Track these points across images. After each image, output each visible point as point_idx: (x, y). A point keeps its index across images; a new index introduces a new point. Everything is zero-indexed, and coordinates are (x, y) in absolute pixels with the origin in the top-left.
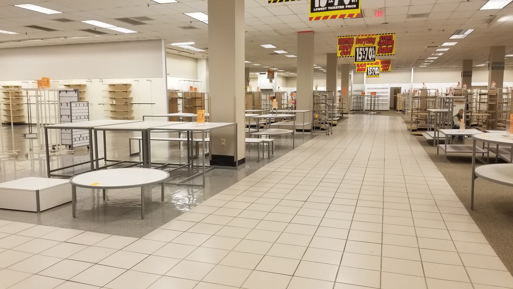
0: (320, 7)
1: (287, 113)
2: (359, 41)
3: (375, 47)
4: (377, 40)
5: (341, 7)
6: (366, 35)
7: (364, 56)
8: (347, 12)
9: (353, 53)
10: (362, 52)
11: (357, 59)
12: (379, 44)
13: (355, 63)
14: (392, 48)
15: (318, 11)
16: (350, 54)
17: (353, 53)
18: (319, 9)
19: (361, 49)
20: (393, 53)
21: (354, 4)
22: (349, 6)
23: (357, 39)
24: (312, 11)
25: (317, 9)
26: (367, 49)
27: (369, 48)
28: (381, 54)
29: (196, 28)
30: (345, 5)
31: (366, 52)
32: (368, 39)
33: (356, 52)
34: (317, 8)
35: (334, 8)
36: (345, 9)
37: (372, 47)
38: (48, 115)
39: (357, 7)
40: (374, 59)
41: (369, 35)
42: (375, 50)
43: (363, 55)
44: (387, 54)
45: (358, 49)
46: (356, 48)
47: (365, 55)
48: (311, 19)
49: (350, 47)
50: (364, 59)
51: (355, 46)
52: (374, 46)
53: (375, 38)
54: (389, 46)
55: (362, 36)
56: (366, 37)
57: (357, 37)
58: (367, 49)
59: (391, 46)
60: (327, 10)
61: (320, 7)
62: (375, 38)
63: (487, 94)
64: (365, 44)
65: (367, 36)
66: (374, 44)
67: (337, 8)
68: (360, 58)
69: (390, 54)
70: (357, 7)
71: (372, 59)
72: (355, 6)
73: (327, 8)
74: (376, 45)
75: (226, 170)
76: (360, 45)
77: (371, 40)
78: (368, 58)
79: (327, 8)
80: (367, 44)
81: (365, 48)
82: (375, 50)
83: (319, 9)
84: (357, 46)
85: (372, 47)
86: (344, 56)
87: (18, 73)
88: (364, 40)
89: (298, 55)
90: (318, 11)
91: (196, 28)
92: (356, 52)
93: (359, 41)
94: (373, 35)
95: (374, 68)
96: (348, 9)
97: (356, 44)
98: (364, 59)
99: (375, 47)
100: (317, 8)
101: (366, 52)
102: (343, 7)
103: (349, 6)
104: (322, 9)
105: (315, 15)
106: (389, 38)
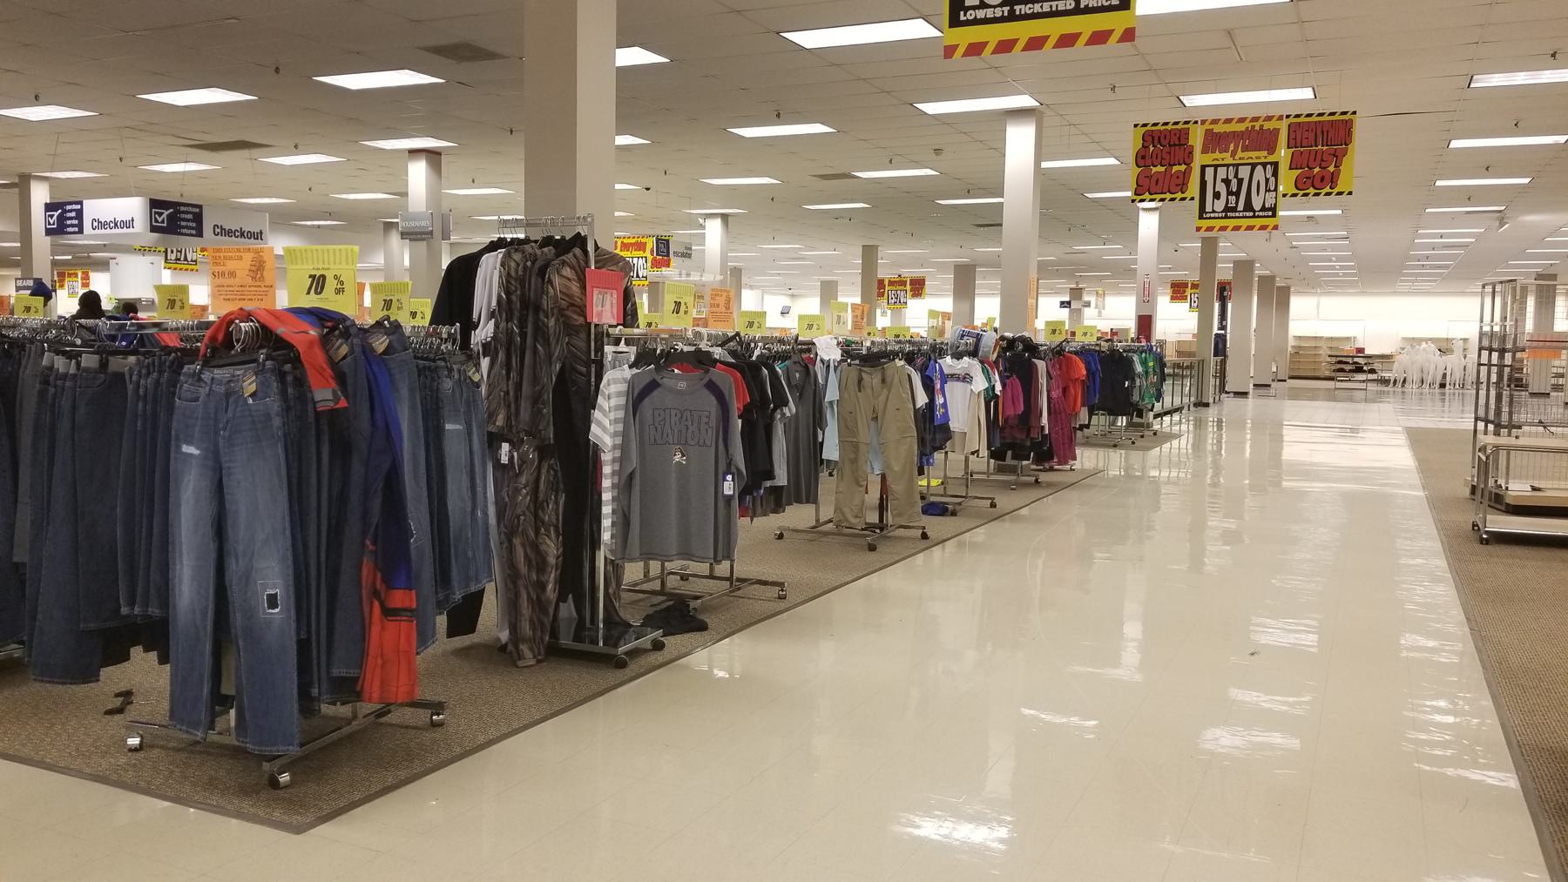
1: (485, 478)
8: (1258, 222)
9: (1193, 188)
10: (1227, 182)
11: (1209, 208)
17: (1193, 188)
18: (981, 14)
19: (1222, 173)
23: (1209, 133)
24: (1201, 217)
25: (971, 15)
26: (1244, 172)
27: (1254, 166)
31: (1240, 181)
33: (1203, 184)
34: (974, 8)
37: (1264, 165)
38: (1488, 300)
41: (1255, 119)
42: (1275, 174)
43: (1230, 193)
44: (1169, 196)
45: (1209, 172)
46: (1203, 168)
47: (1237, 194)
50: (1234, 209)
52: (1271, 159)
54: (1175, 169)
56: (1241, 127)
57: (1207, 126)
59: (1183, 167)
60: (1012, 17)
64: (1240, 154)
65: (1248, 124)
66: (1272, 149)
68: (1220, 205)
69: (1179, 195)
70: (1274, 215)
71: (1263, 209)
73: (1012, 11)
76: (1217, 155)
78: (1249, 206)
79: (1012, 11)
80: (1246, 154)
83: (981, 14)
84: (1208, 159)
85: (1264, 165)
86: (1312, 191)
92: (1203, 184)
95: (1244, 172)
97: (1205, 151)
98: (1234, 209)
99: (1276, 165)
100: (974, 8)
104: (989, 13)
105: (1205, 223)
106: (1175, 140)
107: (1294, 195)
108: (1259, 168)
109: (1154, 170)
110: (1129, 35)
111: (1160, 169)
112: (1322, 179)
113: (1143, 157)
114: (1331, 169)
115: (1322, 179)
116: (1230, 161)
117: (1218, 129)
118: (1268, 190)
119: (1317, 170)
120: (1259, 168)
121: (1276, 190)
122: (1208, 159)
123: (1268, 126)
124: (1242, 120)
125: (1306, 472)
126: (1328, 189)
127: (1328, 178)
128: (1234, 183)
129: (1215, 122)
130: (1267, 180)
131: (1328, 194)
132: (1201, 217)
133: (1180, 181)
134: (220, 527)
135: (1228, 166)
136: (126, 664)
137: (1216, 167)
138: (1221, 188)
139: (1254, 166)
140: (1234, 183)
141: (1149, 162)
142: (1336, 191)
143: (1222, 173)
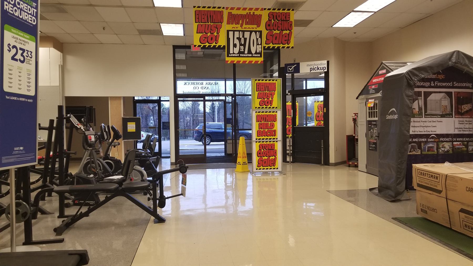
0: (234, 53)
2: (233, 19)
3: (261, 32)
4: (265, 19)
5: (249, 55)
6: (245, 9)
7: (242, 47)
10: (239, 39)
11: (231, 52)
12: (268, 26)
14: (289, 35)
15: (232, 57)
18: (233, 55)
19: (237, 34)
20: (291, 45)
21: (258, 53)
22: (255, 55)
23: (230, 14)
25: (231, 55)
26: (247, 35)
27: (251, 32)
30: (252, 54)
31: (245, 39)
32: (248, 16)
35: (244, 55)
36: (252, 57)
37: (256, 32)
41: (251, 9)
42: (261, 36)
43: (241, 45)
45: (231, 34)
46: (228, 31)
47: (244, 45)
48: (276, 112)
49: (218, 28)
50: (243, 53)
51: (225, 27)
52: (258, 29)
53: (260, 16)
54: (284, 32)
55: (238, 9)
56: (244, 13)
57: (229, 10)
58: (247, 35)
59: (288, 32)
60: (239, 56)
61: (234, 53)
62: (260, 16)
64: (244, 26)
66: (259, 25)
67: (246, 55)
68: (236, 50)
71: (256, 53)
72: (259, 55)
74: (262, 27)
75: (41, 239)
76: (234, 25)
77: (254, 19)
78: (250, 52)
80: (248, 26)
81: (243, 32)
82: (261, 36)
83: (233, 55)
84: (230, 27)
85: (256, 32)
87: (471, 126)
88: (242, 17)
90: (232, 57)
93: (233, 19)
94: (257, 9)
96: (254, 57)
97: (228, 23)
98: (243, 53)
99: (261, 32)
101: (245, 39)
102: (251, 55)
103: (255, 55)
104: (235, 55)
106: (283, 18)
108: (253, 33)
109: (275, 32)
110: (194, 7)
112: (212, 39)
113: (269, 25)
114: (215, 34)
115: (212, 39)
116: (240, 29)
117: (234, 12)
118: (258, 44)
120: (253, 33)
121: (261, 44)
122: (230, 27)
123: (257, 13)
124: (245, 9)
125: (246, 180)
127: (214, 38)
128: (243, 39)
129: (232, 9)
130: (257, 39)
132: (228, 56)
133: (287, 38)
134: (421, 191)
135: (239, 31)
136: (89, 254)
137: (234, 31)
138: (237, 42)
139: (251, 32)
140: (243, 39)
141: (272, 28)
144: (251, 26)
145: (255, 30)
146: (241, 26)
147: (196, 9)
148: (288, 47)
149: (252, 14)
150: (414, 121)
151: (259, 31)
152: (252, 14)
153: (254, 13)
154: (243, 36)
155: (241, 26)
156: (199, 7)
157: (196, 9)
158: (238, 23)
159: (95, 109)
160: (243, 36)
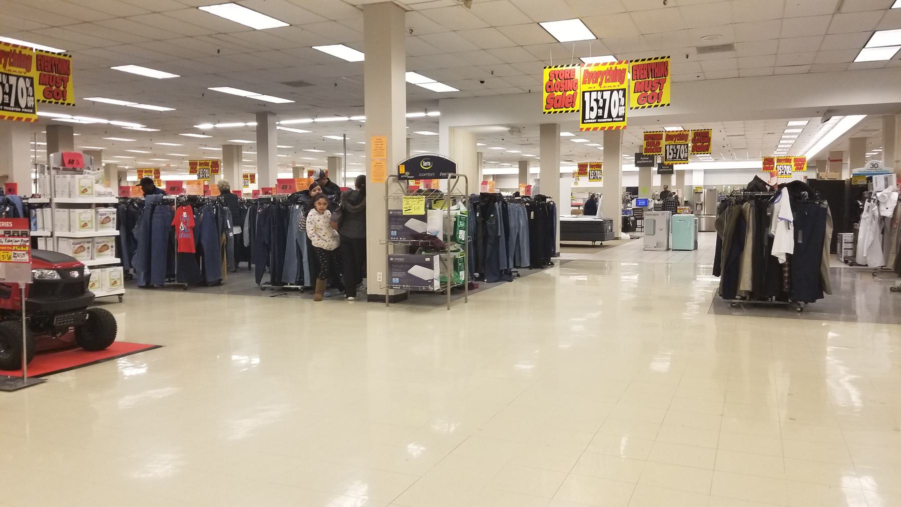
7: (600, 111)
9: (578, 105)
10: (597, 101)
11: (587, 117)
13: (582, 126)
16: (659, 99)
17: (578, 105)
19: (594, 95)
21: (30, 108)
24: (583, 123)
26: (607, 95)
27: (612, 91)
28: (552, 110)
29: (310, 85)
30: (20, 107)
31: (605, 101)
32: (609, 72)
37: (25, 78)
39: (624, 120)
40: (623, 117)
42: (32, 85)
43: (599, 108)
44: (564, 109)
46: (584, 93)
47: (603, 108)
50: (602, 117)
52: (622, 87)
54: (568, 93)
56: (604, 68)
59: (572, 92)
63: (115, 205)
64: (604, 84)
65: (608, 66)
69: (570, 109)
70: (624, 120)
71: (618, 117)
76: (591, 85)
78: (610, 116)
80: (608, 84)
81: (602, 91)
84: (667, 143)
85: (618, 90)
86: (647, 105)
89: (48, 142)
91: (310, 85)
98: (602, 117)
99: (32, 79)
101: (605, 101)
107: (637, 108)
108: (615, 92)
109: (556, 94)
111: (560, 93)
114: (658, 91)
119: (649, 92)
120: (615, 92)
121: (33, 96)
126: (656, 103)
130: (27, 89)
131: (656, 106)
132: (583, 123)
137: (590, 92)
138: (594, 104)
139: (612, 91)
140: (7, 86)
142: (660, 104)
143: (594, 95)
144: (18, 69)
145: (23, 74)
146: (600, 85)
147: (634, 63)
148: (573, 111)
149: (17, 52)
150: (579, 206)
151: (29, 78)
152: (17, 52)
153: (20, 52)
154: (8, 82)
155: (600, 85)
156: (637, 61)
157: (634, 63)
158: (596, 82)
159: (716, 273)
160: (8, 82)
